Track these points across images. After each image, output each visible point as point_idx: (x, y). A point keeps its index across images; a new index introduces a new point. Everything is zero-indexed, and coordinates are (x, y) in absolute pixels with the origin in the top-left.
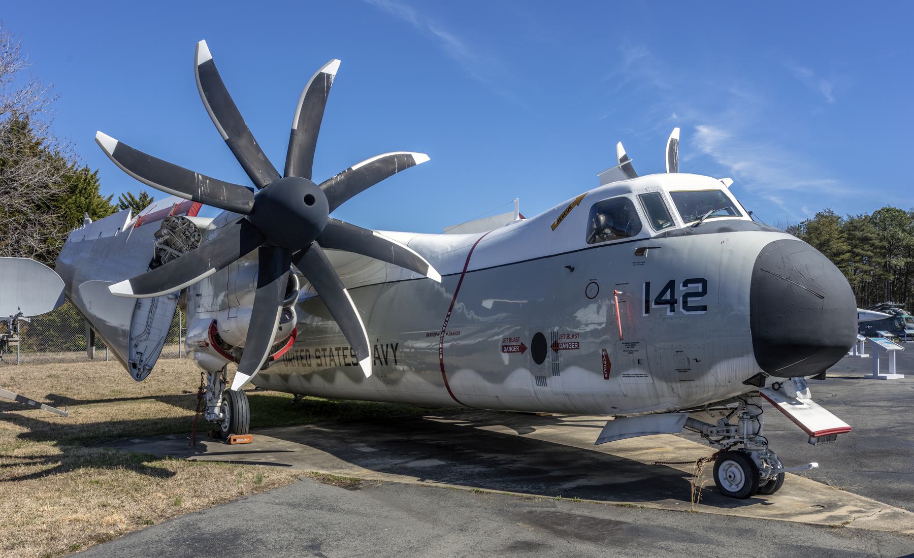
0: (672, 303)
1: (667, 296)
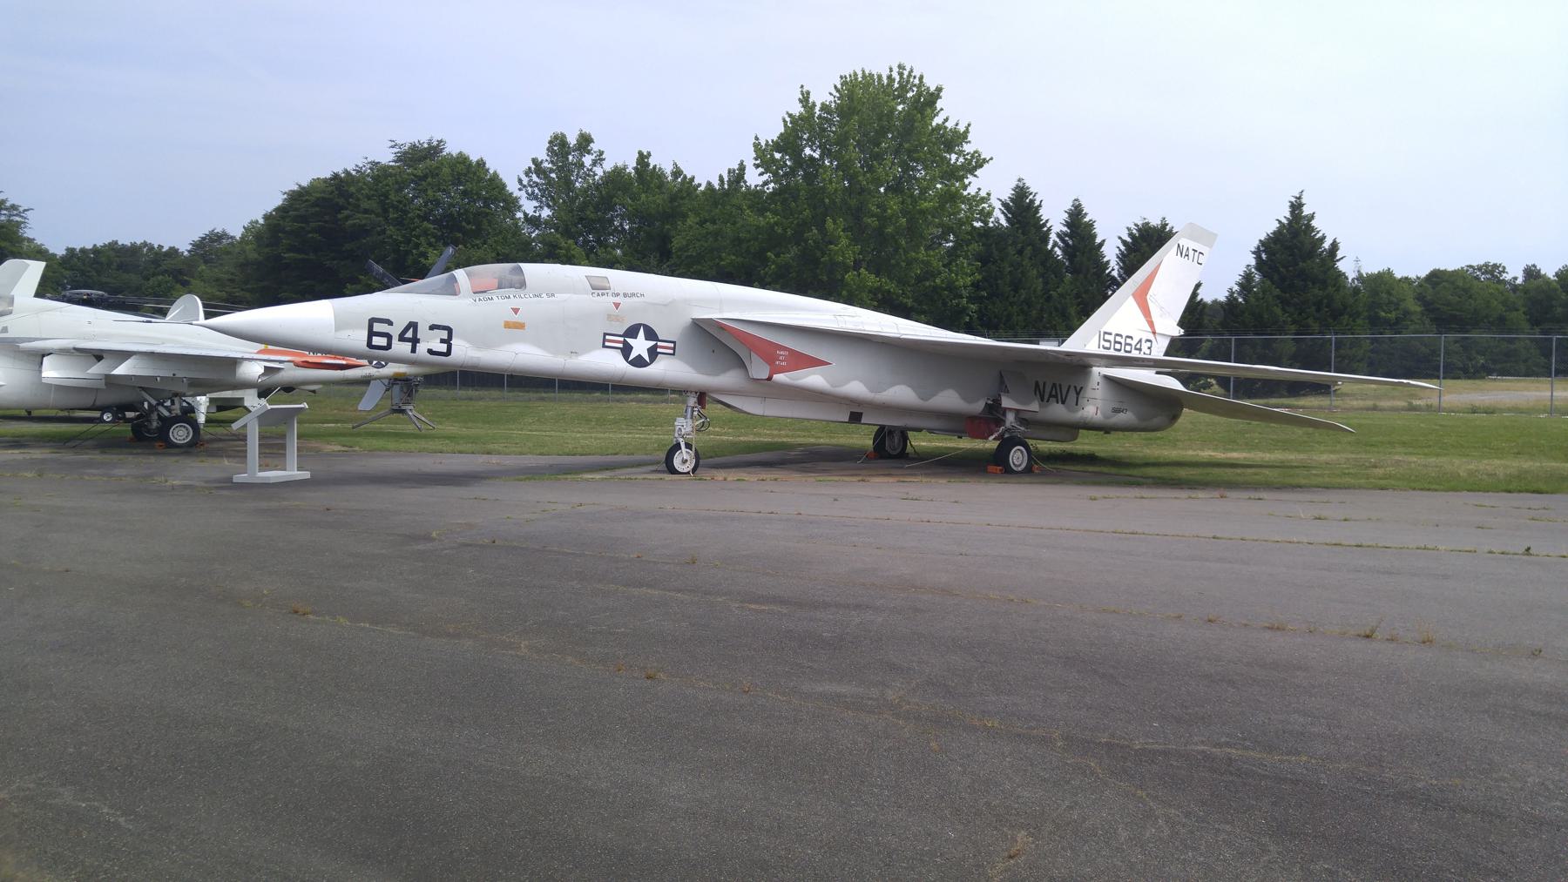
0: (415, 341)
1: (409, 334)
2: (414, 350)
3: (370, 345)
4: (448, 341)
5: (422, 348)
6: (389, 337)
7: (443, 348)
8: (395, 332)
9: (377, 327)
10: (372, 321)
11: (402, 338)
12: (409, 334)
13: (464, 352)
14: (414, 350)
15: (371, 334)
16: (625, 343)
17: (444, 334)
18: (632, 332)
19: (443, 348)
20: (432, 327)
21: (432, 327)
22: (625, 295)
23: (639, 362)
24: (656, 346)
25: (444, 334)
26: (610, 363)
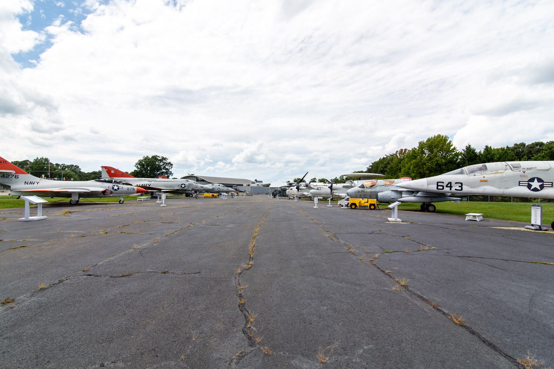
0: (451, 187)
1: (449, 185)
2: (451, 189)
3: (437, 188)
4: (461, 187)
5: (453, 189)
6: (443, 186)
7: (460, 188)
8: (445, 185)
9: (439, 184)
10: (438, 183)
11: (447, 186)
12: (449, 185)
13: (466, 189)
14: (451, 189)
15: (438, 186)
16: (528, 184)
17: (460, 185)
18: (539, 180)
19: (460, 188)
20: (456, 183)
21: (456, 183)
22: (528, 169)
23: (535, 190)
24: (543, 184)
25: (460, 185)
26: (524, 191)
